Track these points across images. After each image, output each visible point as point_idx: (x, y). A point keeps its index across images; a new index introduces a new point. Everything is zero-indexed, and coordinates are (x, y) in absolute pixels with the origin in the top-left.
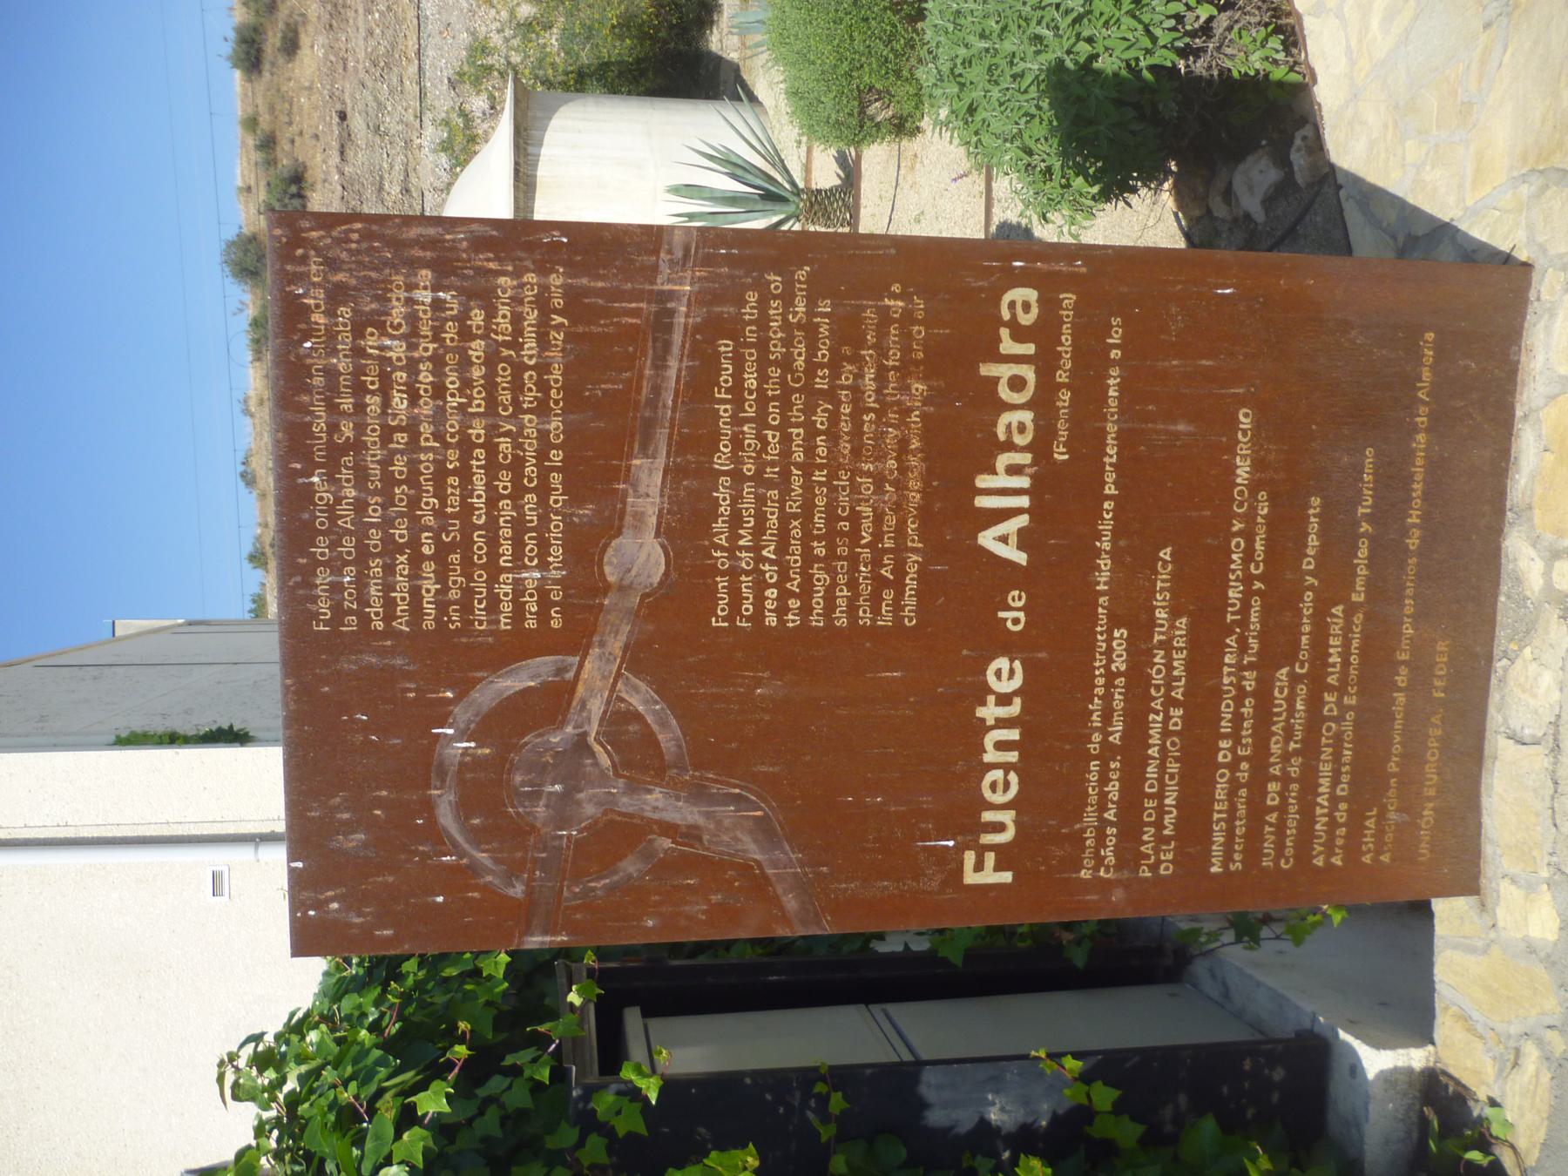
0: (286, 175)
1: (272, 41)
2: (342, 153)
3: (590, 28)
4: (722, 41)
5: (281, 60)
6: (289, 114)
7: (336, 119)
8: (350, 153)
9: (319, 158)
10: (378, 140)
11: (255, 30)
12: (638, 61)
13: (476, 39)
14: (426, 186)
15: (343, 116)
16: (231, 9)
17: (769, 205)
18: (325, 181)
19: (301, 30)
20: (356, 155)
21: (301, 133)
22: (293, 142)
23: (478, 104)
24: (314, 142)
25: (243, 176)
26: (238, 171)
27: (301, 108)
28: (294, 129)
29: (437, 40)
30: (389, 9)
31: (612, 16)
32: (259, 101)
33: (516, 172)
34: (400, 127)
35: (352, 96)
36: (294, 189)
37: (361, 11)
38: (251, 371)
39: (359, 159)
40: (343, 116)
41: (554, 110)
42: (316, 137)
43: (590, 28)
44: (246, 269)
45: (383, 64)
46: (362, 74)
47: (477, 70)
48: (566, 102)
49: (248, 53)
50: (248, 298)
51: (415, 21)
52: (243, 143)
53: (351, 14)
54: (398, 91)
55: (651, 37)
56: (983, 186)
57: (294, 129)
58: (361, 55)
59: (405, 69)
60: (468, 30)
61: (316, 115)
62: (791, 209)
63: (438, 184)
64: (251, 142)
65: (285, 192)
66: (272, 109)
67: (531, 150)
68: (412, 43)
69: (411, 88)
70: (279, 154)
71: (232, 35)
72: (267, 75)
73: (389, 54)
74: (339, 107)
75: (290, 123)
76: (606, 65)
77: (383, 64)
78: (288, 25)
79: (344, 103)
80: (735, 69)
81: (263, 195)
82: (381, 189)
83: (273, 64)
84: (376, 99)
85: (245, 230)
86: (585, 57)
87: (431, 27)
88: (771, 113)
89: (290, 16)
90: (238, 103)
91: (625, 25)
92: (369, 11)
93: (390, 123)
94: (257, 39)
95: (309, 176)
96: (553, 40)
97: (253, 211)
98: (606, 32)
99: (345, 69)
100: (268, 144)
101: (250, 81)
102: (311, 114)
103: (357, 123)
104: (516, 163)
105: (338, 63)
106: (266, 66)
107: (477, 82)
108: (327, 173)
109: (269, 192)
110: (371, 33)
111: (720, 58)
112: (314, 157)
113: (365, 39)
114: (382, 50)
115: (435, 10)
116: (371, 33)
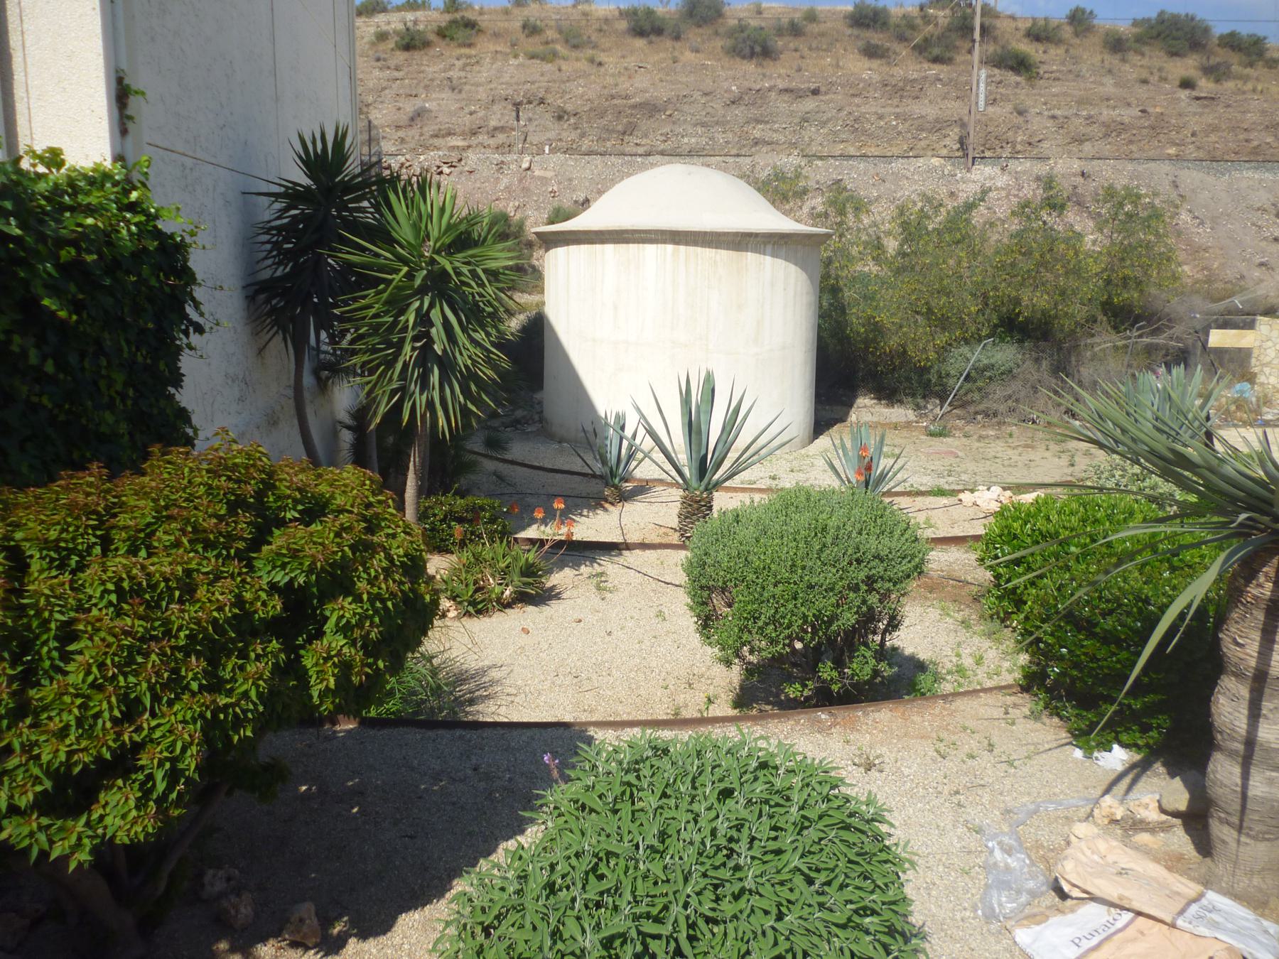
0: (770, 43)
1: (876, 37)
2: (786, 90)
3: (872, 299)
4: (866, 410)
5: (860, 43)
6: (818, 49)
7: (813, 86)
8: (786, 97)
9: (782, 71)
10: (797, 120)
11: (884, 24)
12: (848, 338)
13: (870, 203)
14: (757, 158)
15: (815, 92)
16: (901, 6)
17: (695, 464)
18: (764, 75)
19: (884, 61)
20: (785, 102)
21: (803, 57)
22: (796, 50)
23: (818, 202)
24: (795, 67)
25: (770, 8)
26: (774, 5)
27: (822, 58)
28: (806, 52)
29: (872, 171)
30: (899, 133)
31: (883, 317)
32: (828, 24)
33: (750, 235)
34: (806, 139)
35: (832, 101)
36: (758, 49)
37: (898, 110)
38: (612, 7)
39: (781, 104)
40: (815, 92)
41: (804, 268)
42: (799, 70)
43: (872, 299)
44: (694, 7)
45: (856, 127)
46: (848, 109)
47: (843, 201)
48: (811, 278)
49: (866, 17)
50: (672, 7)
51: (889, 154)
52: (795, 10)
53: (896, 101)
54: (835, 138)
55: (867, 348)
56: (625, 717)
57: (806, 52)
58: (863, 109)
59: (853, 145)
60: (879, 196)
61: (817, 71)
62: (694, 483)
63: (758, 168)
64: (797, 15)
65: (755, 42)
66: (822, 35)
67: (769, 248)
68: (873, 151)
69: (839, 149)
70: (787, 39)
71: (880, 5)
72: (849, 31)
73: (865, 131)
74: (823, 89)
75: (810, 49)
76: (843, 310)
77: (856, 127)
78: (888, 49)
79: (826, 93)
80: (842, 419)
81: (754, 23)
82: (758, 121)
83: (858, 37)
84: (829, 120)
85: (726, 8)
86: (848, 294)
87: (882, 167)
88: (803, 451)
89: (895, 53)
90: (828, 8)
91: (876, 329)
92: (897, 116)
93: (810, 131)
94: (878, 26)
95: (768, 62)
96: (871, 268)
97: (742, 15)
98: (869, 312)
99: (853, 95)
100: (795, 30)
101: (845, 17)
102: (817, 67)
103: (810, 104)
104: (757, 235)
105: (857, 90)
106: (856, 32)
107: (832, 203)
108: (771, 77)
109: (755, 29)
110: (881, 117)
111: (851, 406)
112: (784, 67)
113: (876, 113)
114: (868, 126)
115: (895, 170)
116: (881, 117)
